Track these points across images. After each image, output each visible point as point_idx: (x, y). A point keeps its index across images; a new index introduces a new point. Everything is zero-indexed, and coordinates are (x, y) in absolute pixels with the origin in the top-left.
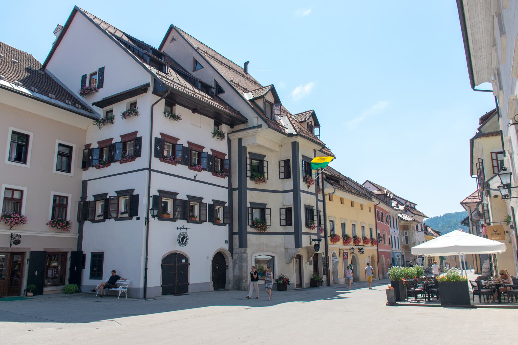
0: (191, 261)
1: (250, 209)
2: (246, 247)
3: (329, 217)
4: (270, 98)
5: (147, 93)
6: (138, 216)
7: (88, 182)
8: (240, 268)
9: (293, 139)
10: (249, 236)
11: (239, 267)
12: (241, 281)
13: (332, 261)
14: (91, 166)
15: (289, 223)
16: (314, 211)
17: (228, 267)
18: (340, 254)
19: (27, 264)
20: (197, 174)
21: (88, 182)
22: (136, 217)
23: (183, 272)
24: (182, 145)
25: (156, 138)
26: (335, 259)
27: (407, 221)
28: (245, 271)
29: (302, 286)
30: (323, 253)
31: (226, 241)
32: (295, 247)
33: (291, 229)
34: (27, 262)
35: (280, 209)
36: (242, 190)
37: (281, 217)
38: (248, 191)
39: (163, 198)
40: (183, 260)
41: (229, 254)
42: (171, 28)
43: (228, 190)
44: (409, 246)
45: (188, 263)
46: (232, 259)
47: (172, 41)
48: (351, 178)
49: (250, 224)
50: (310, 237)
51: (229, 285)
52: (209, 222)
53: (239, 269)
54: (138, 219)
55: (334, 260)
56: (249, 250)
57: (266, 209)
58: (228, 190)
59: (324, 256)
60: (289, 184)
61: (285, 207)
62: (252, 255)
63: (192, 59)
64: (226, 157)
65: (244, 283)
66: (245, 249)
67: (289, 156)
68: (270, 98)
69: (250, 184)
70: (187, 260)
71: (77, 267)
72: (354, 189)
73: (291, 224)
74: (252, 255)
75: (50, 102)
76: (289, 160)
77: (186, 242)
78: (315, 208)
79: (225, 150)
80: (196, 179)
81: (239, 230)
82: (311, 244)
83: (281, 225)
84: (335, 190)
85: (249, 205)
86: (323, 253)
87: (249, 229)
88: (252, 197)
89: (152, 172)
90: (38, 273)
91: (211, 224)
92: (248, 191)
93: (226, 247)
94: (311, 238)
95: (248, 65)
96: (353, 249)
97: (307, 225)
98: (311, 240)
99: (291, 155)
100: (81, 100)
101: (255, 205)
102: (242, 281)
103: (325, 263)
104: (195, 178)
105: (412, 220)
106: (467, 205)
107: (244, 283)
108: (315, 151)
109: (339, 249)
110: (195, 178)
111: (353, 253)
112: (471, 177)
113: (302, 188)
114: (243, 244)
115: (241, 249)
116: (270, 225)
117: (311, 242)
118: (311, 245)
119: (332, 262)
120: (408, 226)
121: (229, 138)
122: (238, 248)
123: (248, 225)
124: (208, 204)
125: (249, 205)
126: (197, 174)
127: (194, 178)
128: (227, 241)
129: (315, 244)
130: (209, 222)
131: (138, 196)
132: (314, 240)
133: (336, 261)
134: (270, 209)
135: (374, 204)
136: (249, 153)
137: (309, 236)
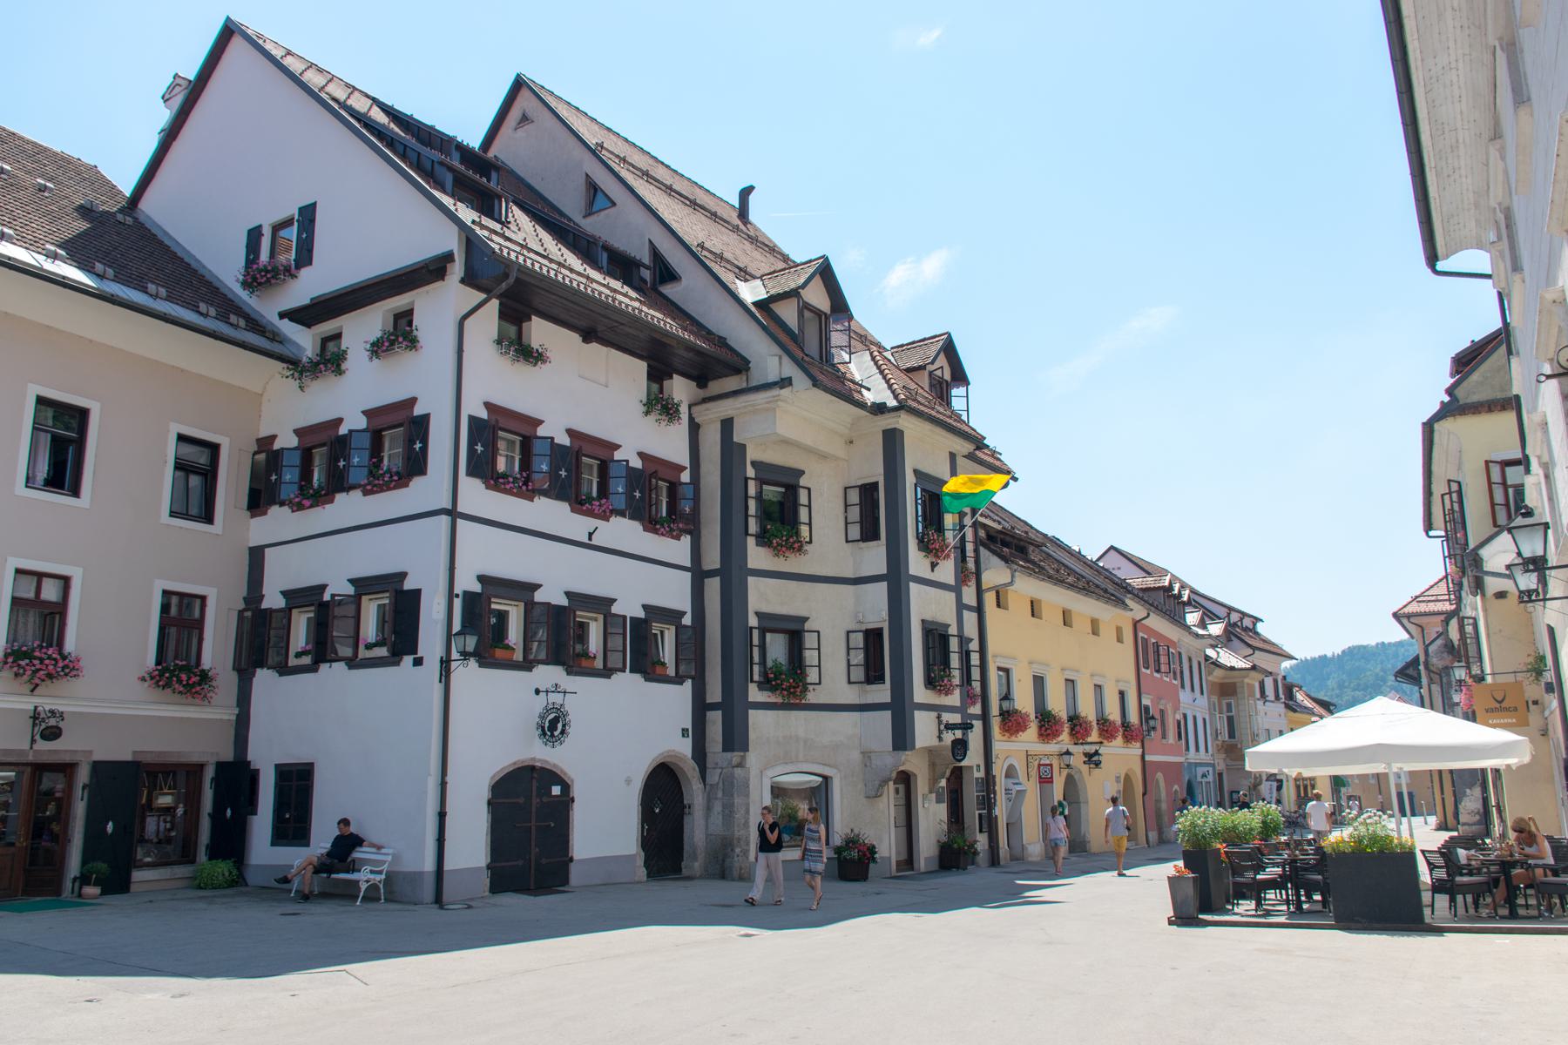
0: (577, 792)
1: (756, 633)
2: (745, 747)
3: (995, 656)
4: (817, 297)
5: (444, 280)
6: (416, 654)
7: (267, 550)
8: (727, 811)
9: (887, 422)
10: (754, 715)
11: (723, 808)
12: (729, 850)
13: (1006, 790)
14: (275, 503)
15: (873, 674)
16: (951, 638)
17: (689, 807)
18: (1030, 770)
19: (82, 800)
20: (597, 528)
21: (267, 550)
22: (412, 657)
23: (553, 825)
24: (552, 439)
25: (472, 419)
26: (1015, 784)
27: (1232, 668)
28: (743, 821)
29: (916, 865)
30: (978, 766)
31: (683, 730)
32: (894, 749)
33: (882, 693)
34: (83, 794)
35: (848, 632)
36: (733, 575)
37: (851, 657)
38: (751, 580)
39: (493, 600)
40: (553, 787)
41: (694, 769)
42: (519, 85)
43: (689, 574)
44: (1239, 746)
45: (569, 796)
46: (702, 786)
47: (519, 124)
48: (1061, 539)
49: (756, 677)
50: (939, 717)
51: (694, 863)
52: (631, 671)
53: (723, 816)
54: (418, 662)
55: (1011, 786)
56: (753, 758)
57: (806, 634)
58: (689, 574)
59: (981, 774)
60: (874, 558)
61: (864, 627)
62: (761, 772)
63: (582, 180)
64: (685, 477)
65: (740, 858)
66: (742, 754)
67: (874, 471)
68: (817, 297)
69: (758, 556)
70: (566, 788)
71: (232, 810)
72: (1071, 571)
73: (880, 679)
74: (761, 772)
75: (151, 309)
76: (875, 485)
77: (563, 732)
78: (953, 630)
79: (680, 455)
80: (594, 542)
81: (723, 696)
82: (940, 738)
83: (850, 682)
84: (1013, 576)
85: (753, 621)
86: (978, 766)
87: (755, 694)
88: (763, 597)
89: (460, 522)
90: (114, 828)
91: (638, 677)
92: (751, 580)
93: (685, 747)
94: (940, 722)
95: (750, 197)
96: (1068, 753)
97: (930, 683)
98: (942, 727)
99: (881, 470)
100: (244, 302)
101: (771, 622)
102: (732, 850)
103: (983, 796)
104: (590, 539)
105: (1248, 666)
106: (1412, 620)
107: (738, 856)
108: (952, 456)
109: (1027, 756)
110: (590, 539)
111: (1068, 766)
112: (1426, 537)
113: (914, 569)
114: (736, 739)
115: (729, 755)
116: (818, 682)
117: (940, 732)
118: (941, 743)
119: (1006, 794)
120: (1234, 684)
121: (694, 419)
122: (721, 750)
123: (752, 681)
124: (631, 618)
125: (753, 621)
126: (597, 528)
127: (586, 541)
128: (687, 730)
129: (953, 738)
130: (631, 671)
131: (417, 593)
132: (950, 727)
133: (1018, 791)
134: (818, 632)
135: (1133, 619)
136: (754, 464)
137: (935, 714)
